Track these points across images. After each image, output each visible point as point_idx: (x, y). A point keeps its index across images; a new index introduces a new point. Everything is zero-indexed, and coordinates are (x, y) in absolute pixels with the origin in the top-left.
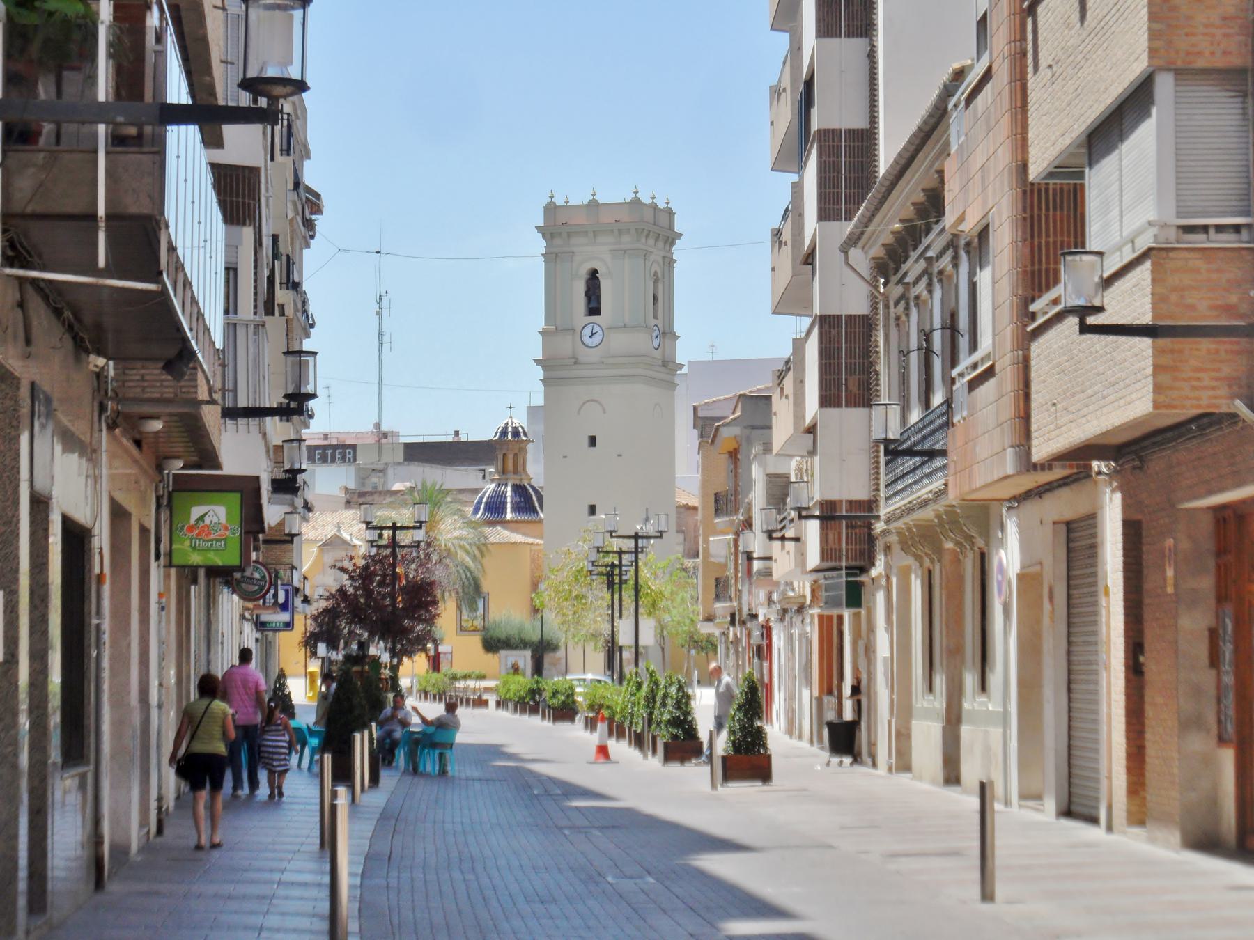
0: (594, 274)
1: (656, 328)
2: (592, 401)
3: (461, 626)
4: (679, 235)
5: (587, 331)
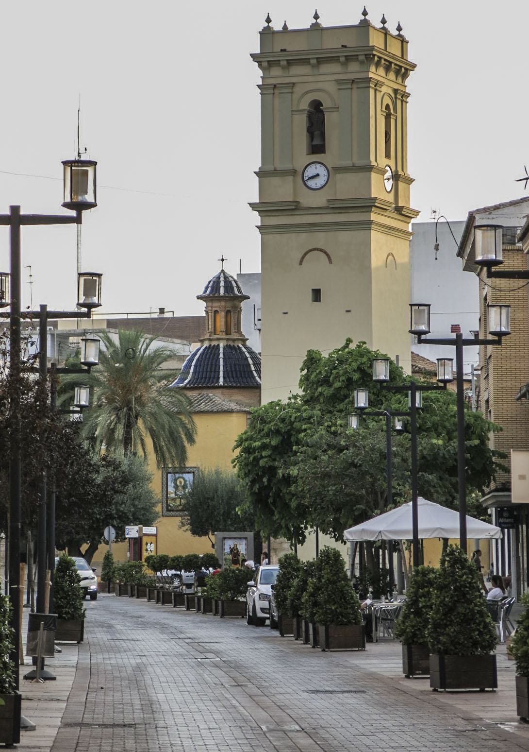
0: (316, 106)
1: (387, 168)
2: (325, 253)
3: (168, 505)
4: (414, 66)
5: (311, 171)
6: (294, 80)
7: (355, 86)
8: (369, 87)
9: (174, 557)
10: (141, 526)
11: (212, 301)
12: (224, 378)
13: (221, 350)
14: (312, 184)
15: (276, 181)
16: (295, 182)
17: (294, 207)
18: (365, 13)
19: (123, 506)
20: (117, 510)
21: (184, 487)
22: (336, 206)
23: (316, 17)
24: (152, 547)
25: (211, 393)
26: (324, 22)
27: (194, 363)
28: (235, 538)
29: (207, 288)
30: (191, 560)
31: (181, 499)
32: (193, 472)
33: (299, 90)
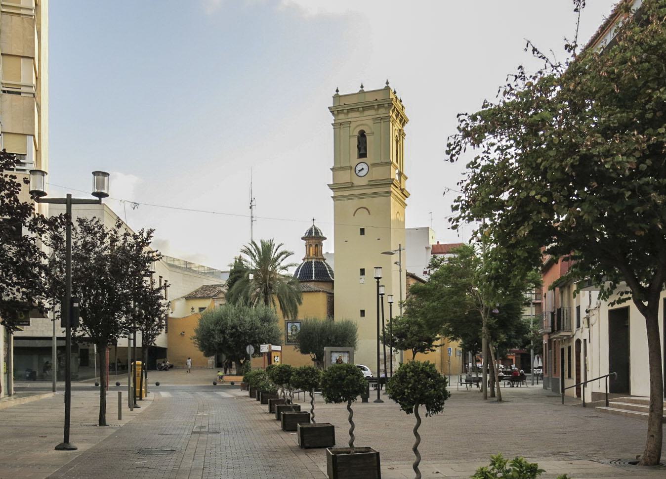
2: (367, 209)
5: (359, 167)
6: (349, 120)
7: (382, 121)
8: (390, 121)
9: (300, 368)
10: (271, 344)
11: (309, 240)
12: (315, 276)
13: (313, 263)
14: (360, 174)
15: (341, 173)
16: (351, 173)
17: (350, 186)
18: (387, 83)
19: (262, 335)
20: (259, 338)
21: (296, 330)
22: (373, 184)
23: (362, 87)
24: (278, 359)
25: (308, 284)
26: (365, 89)
27: (300, 270)
28: (340, 352)
29: (306, 234)
30: (341, 378)
31: (294, 336)
32: (287, 323)
33: (353, 125)
